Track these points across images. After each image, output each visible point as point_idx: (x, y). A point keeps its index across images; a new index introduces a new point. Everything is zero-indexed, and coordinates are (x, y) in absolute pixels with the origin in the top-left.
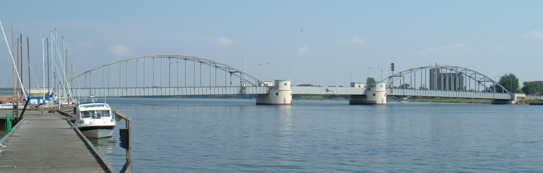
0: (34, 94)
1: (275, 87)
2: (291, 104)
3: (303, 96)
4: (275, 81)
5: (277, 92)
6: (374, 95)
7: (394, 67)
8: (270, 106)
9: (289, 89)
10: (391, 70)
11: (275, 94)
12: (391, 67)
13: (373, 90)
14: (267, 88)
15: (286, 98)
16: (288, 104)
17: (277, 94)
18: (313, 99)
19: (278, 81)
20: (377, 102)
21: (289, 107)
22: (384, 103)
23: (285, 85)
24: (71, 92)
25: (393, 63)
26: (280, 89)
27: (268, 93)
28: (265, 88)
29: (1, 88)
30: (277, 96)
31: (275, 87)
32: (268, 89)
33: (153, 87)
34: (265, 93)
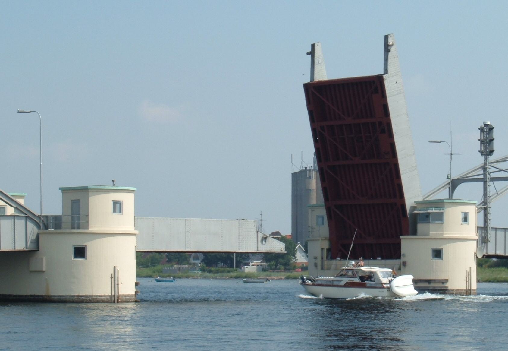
0: (77, 229)
1: (67, 220)
2: (137, 300)
3: (170, 261)
4: (65, 191)
5: (80, 242)
6: (438, 254)
7: (492, 140)
8: (51, 311)
9: (131, 229)
10: (482, 153)
11: (72, 252)
12: (482, 142)
13: (432, 234)
14: (30, 225)
15: (118, 268)
16: (126, 300)
17: (80, 252)
18: (326, 280)
19: (85, 190)
20: (450, 286)
21: (130, 308)
22: (472, 288)
23: (115, 211)
24: (431, 288)
25: (489, 123)
26: (93, 228)
27: (30, 247)
28: (20, 223)
29: (1, 293)
30: (438, 260)
31: (67, 220)
32: (36, 230)
33: (451, 154)
34: (20, 246)
